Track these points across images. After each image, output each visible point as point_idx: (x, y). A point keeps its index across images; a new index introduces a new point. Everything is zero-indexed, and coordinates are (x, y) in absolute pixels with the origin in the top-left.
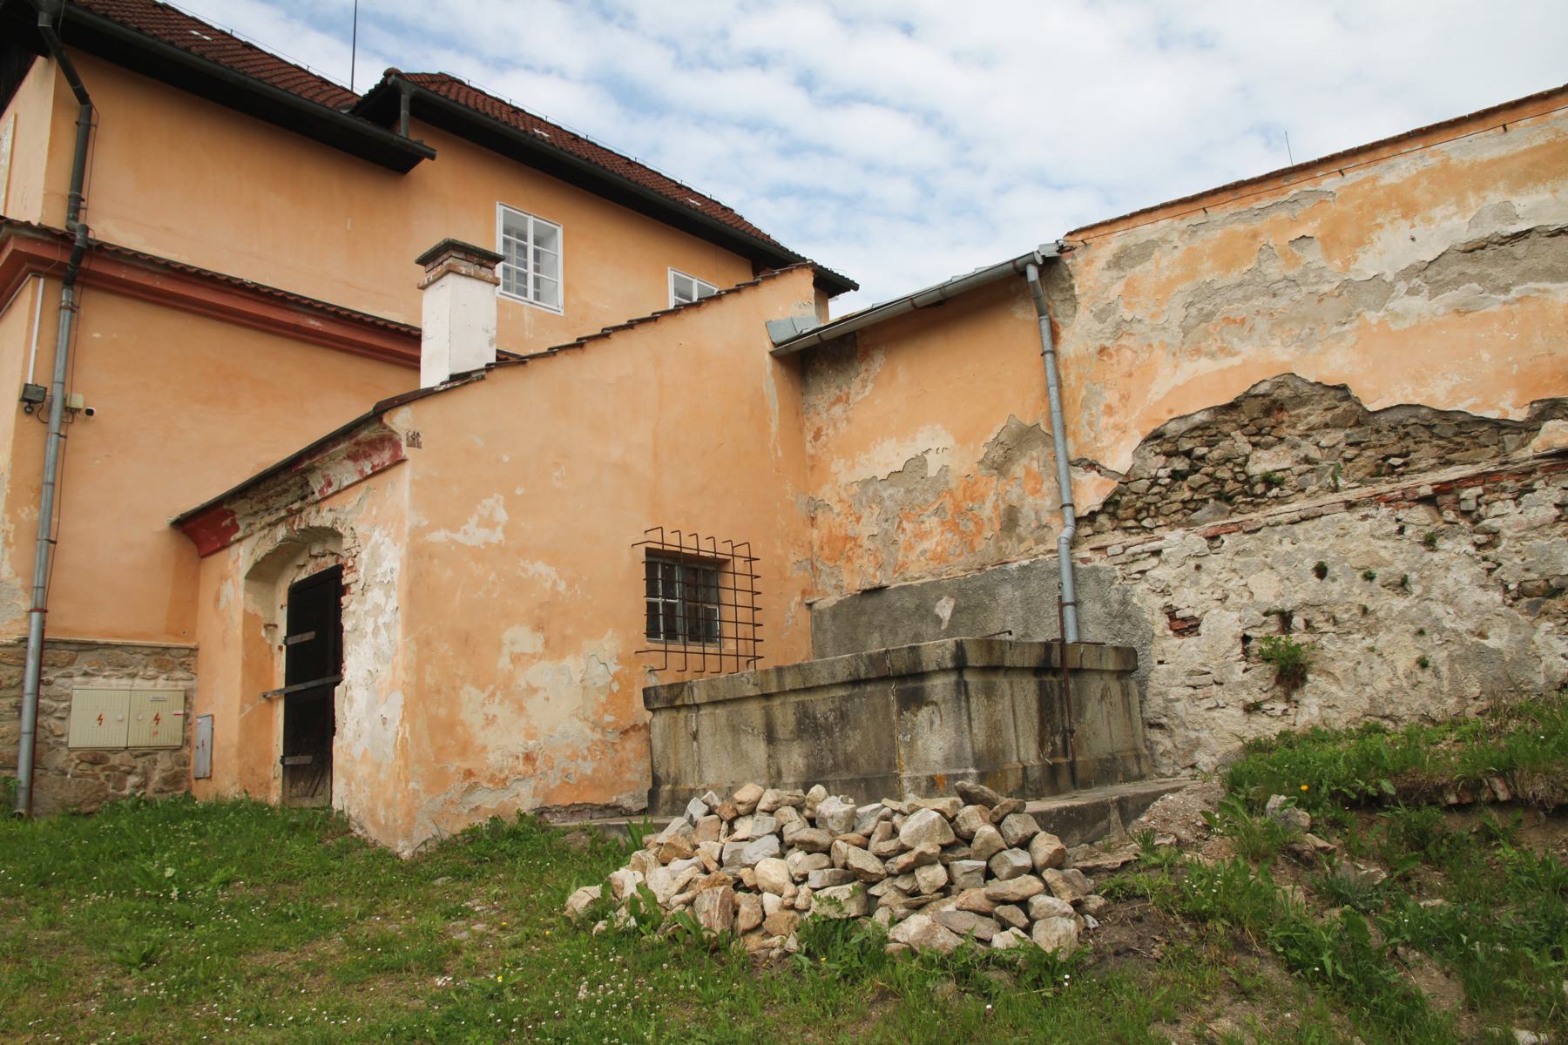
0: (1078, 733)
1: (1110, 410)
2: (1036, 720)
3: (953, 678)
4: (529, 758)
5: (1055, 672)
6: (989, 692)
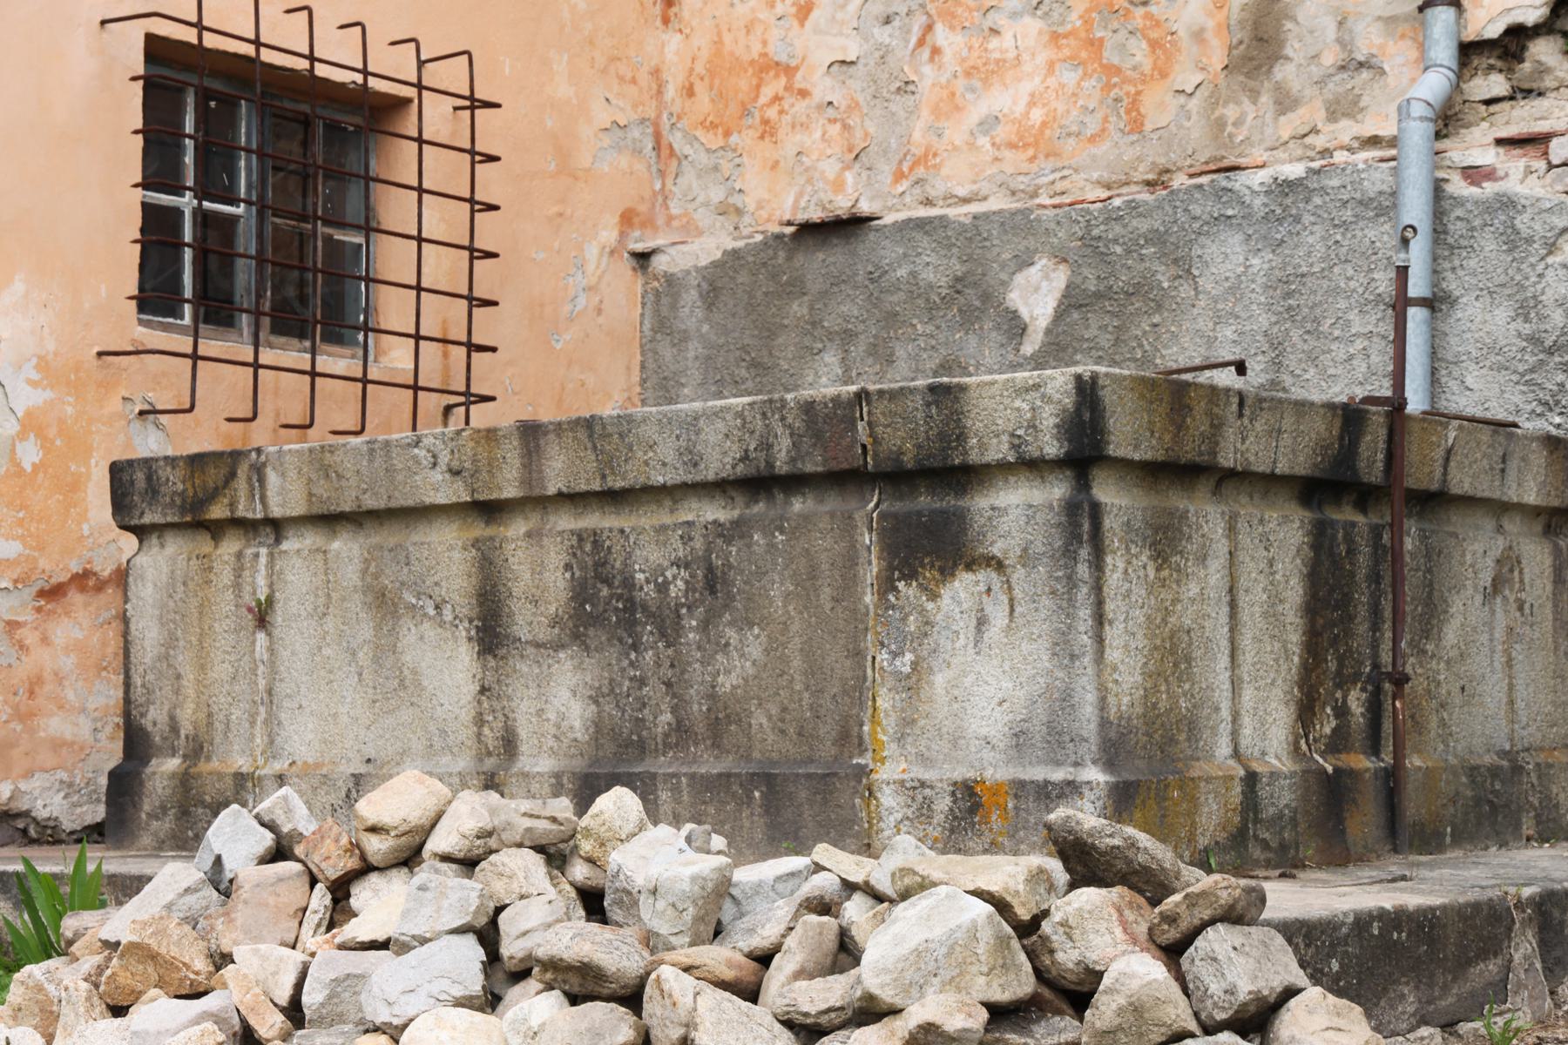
0: (1417, 685)
2: (1295, 638)
3: (1057, 490)
5: (1365, 496)
6: (1164, 540)
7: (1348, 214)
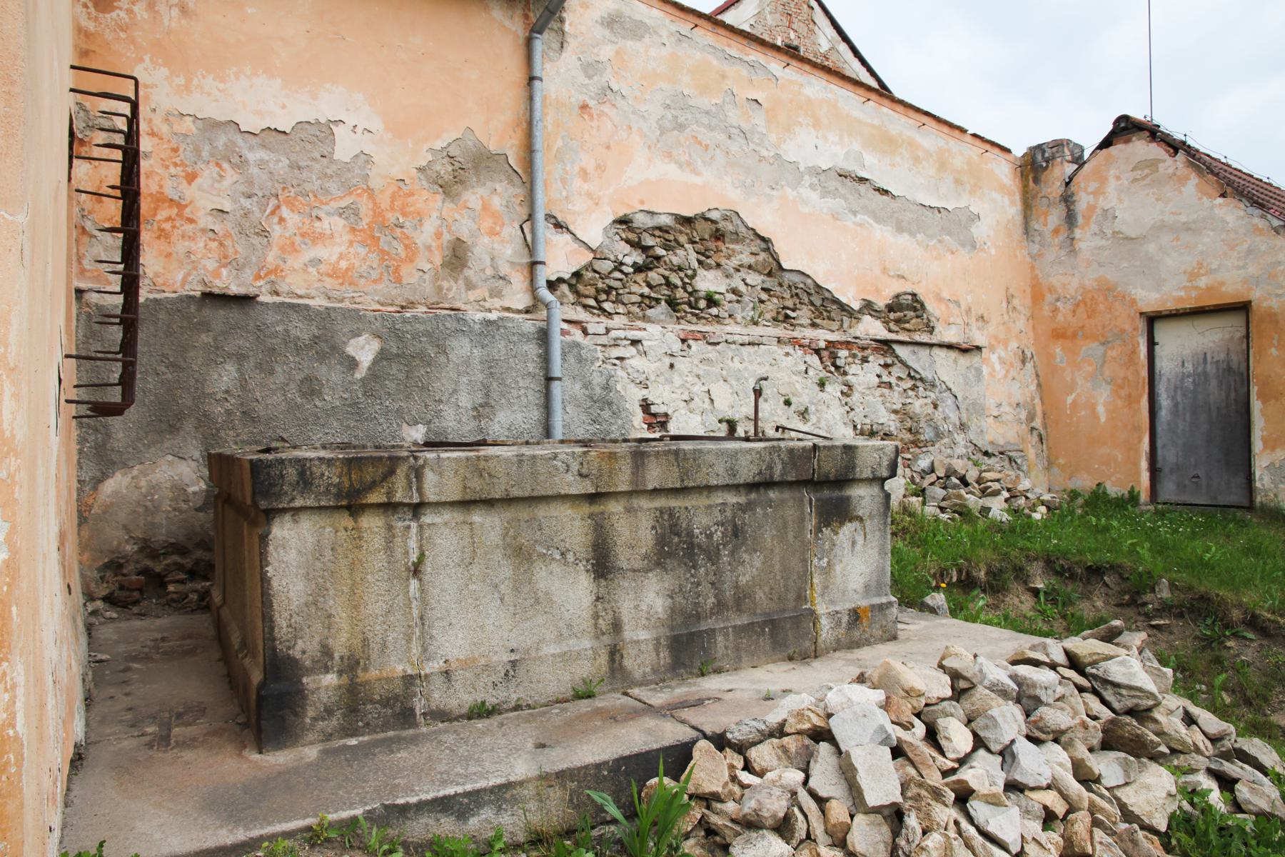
1: (584, 174)
7: (515, 338)
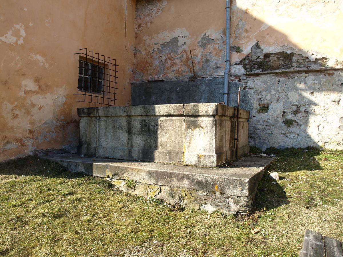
2: (230, 135)
4: (31, 132)
